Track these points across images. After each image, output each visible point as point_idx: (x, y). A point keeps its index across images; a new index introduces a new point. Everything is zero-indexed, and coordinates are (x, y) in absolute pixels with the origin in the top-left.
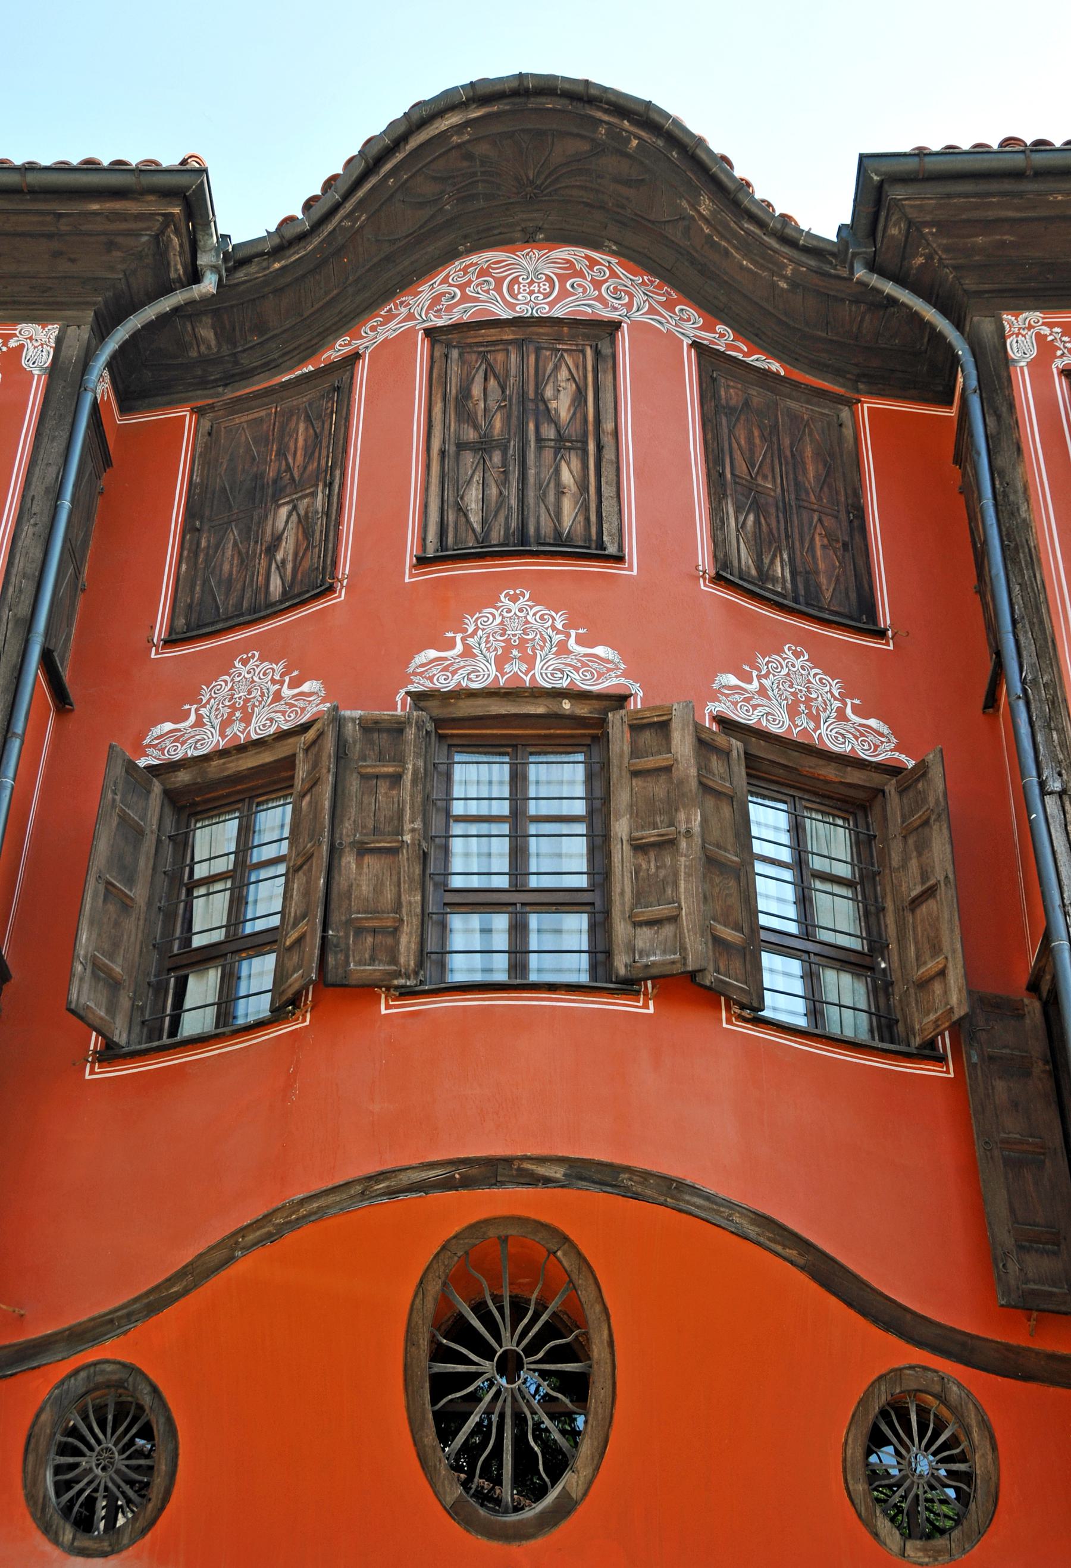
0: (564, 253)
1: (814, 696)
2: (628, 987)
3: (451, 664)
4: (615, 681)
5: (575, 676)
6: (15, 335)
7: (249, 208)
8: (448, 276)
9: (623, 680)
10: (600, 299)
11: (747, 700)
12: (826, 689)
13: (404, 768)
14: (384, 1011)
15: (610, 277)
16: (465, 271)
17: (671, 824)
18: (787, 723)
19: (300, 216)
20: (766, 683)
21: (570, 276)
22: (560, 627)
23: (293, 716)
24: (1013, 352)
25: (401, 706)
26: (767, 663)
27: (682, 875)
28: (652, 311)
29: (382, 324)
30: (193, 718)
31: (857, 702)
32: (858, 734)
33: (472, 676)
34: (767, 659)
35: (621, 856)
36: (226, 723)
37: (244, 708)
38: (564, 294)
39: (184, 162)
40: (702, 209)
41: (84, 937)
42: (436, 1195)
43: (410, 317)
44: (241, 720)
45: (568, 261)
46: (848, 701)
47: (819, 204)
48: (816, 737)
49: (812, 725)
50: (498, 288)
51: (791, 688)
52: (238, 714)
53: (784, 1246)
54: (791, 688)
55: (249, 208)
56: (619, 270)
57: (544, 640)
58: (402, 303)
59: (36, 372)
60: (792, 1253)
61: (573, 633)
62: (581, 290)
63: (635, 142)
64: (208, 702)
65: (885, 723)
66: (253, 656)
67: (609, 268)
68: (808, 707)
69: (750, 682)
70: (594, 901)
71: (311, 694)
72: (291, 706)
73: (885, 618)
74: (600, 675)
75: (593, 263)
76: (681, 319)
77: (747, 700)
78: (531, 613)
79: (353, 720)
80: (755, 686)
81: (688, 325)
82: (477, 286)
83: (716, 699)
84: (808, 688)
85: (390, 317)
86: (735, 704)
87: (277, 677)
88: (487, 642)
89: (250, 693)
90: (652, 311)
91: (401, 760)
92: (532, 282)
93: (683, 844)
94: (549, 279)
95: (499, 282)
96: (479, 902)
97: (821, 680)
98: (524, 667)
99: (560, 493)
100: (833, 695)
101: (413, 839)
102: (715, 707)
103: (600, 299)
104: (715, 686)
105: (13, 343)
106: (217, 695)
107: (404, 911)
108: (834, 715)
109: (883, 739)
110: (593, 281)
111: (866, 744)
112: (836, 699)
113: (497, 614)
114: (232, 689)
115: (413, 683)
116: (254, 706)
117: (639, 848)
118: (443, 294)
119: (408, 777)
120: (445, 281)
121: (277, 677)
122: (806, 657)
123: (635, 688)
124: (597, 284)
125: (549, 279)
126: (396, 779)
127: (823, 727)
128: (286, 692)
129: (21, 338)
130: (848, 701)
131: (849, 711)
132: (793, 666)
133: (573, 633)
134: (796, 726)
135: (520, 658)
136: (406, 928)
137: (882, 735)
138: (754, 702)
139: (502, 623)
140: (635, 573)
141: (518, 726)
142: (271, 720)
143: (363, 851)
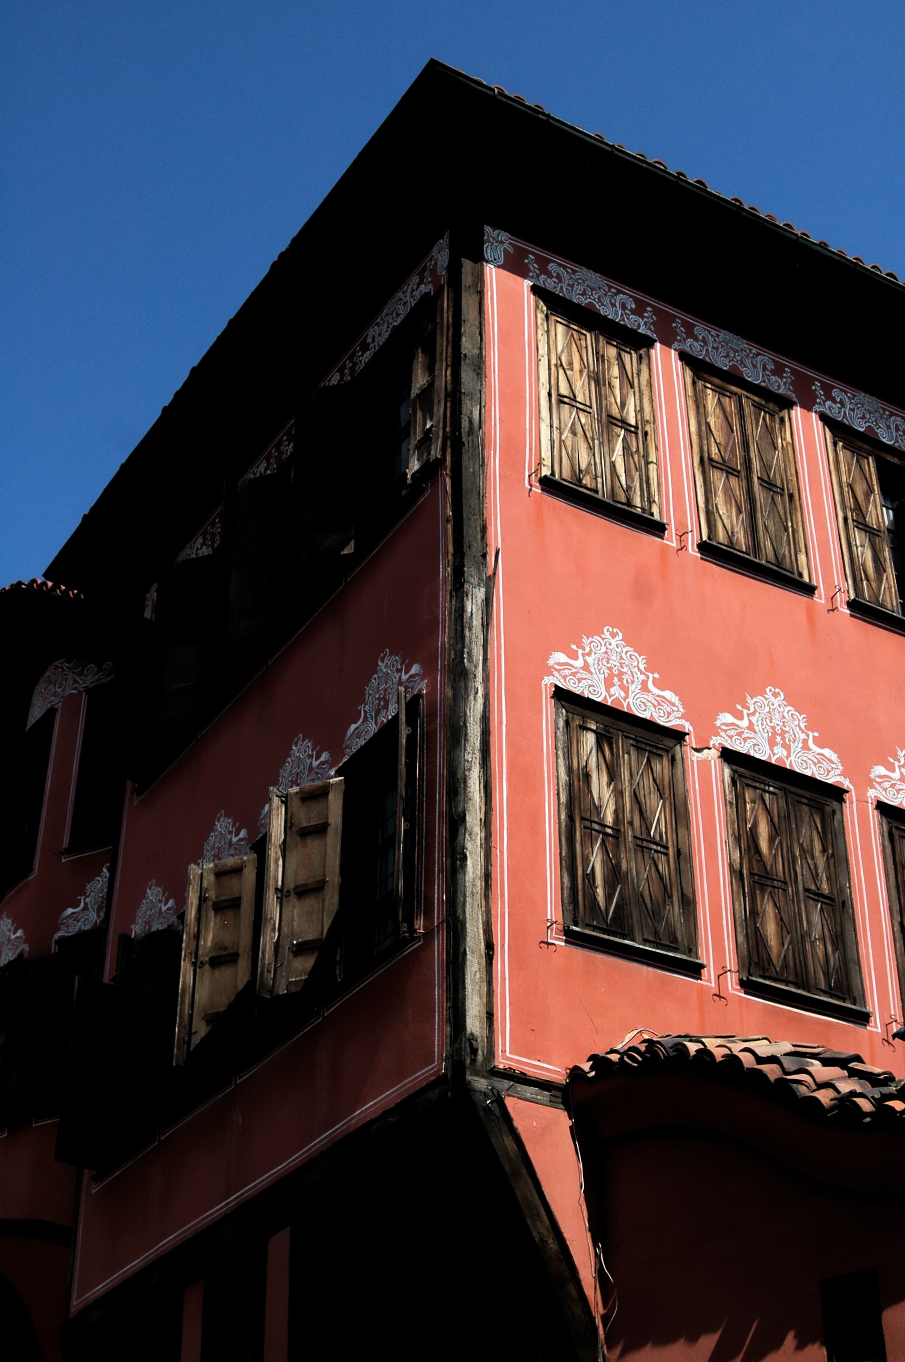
1: (787, 729)
11: (739, 734)
12: (635, 664)
20: (753, 719)
26: (590, 643)
31: (816, 734)
32: (656, 703)
34: (590, 639)
48: (625, 705)
49: (623, 694)
65: (835, 752)
68: (621, 680)
69: (742, 719)
77: (574, 674)
80: (579, 663)
83: (717, 734)
84: (621, 663)
97: (792, 715)
100: (639, 670)
108: (801, 745)
109: (834, 766)
111: (822, 769)
122: (621, 637)
127: (631, 696)
131: (650, 685)
132: (610, 644)
134: (611, 696)
137: (674, 705)
138: (897, 787)
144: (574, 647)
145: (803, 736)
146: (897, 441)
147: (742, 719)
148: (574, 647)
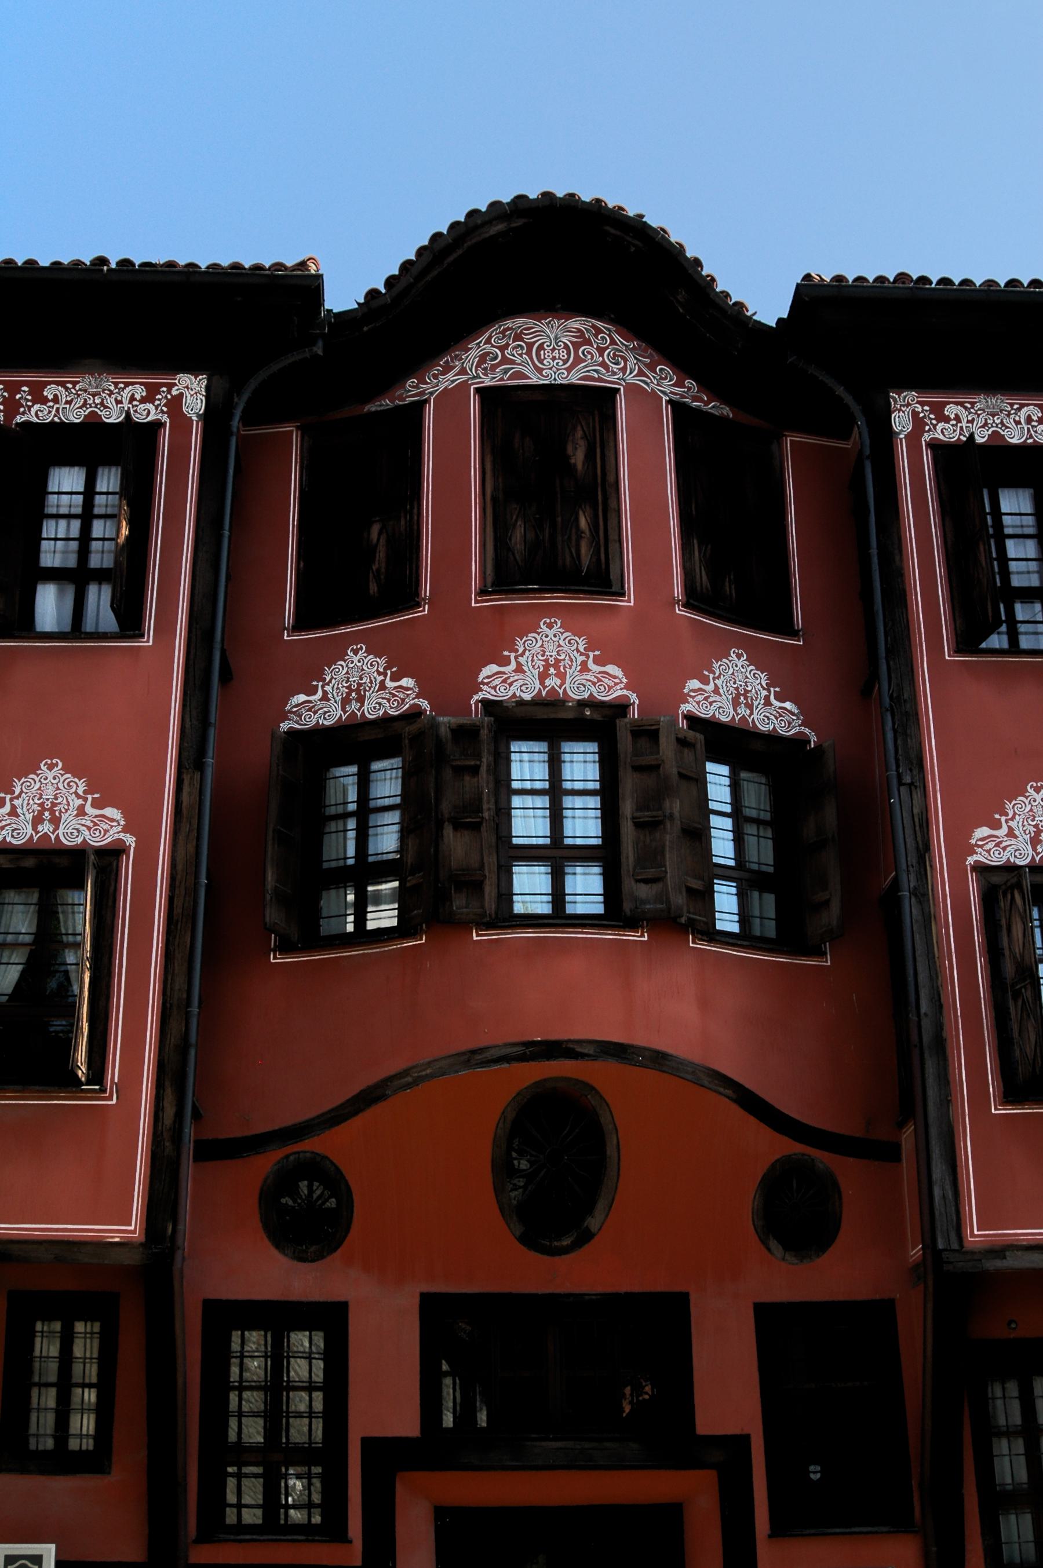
0: (576, 323)
1: (749, 688)
2: (631, 924)
3: (508, 678)
4: (619, 693)
5: (593, 689)
6: (175, 385)
7: (341, 296)
8: (490, 337)
9: (625, 692)
10: (603, 364)
12: (757, 682)
13: (481, 762)
14: (475, 938)
15: (611, 344)
16: (503, 332)
17: (660, 808)
18: (732, 712)
19: (383, 291)
20: (719, 682)
21: (581, 344)
22: (582, 650)
23: (396, 704)
24: (896, 428)
25: (475, 713)
27: (667, 849)
28: (641, 373)
29: (444, 373)
30: (320, 693)
31: (778, 689)
32: (596, 680)
33: (523, 688)
35: (628, 831)
36: (346, 701)
37: (358, 691)
38: (578, 360)
39: (303, 265)
40: (679, 297)
41: (270, 876)
42: (516, 1065)
43: (463, 371)
44: (357, 700)
45: (579, 330)
46: (772, 689)
47: (769, 305)
50: (529, 353)
51: (735, 687)
52: (354, 694)
53: (725, 1088)
54: (735, 687)
55: (341, 296)
56: (617, 338)
57: (571, 660)
58: (457, 356)
59: (195, 418)
60: (728, 1092)
61: (591, 654)
62: (589, 357)
63: (633, 249)
64: (19, 795)
66: (361, 648)
67: (610, 336)
68: (746, 698)
69: (708, 684)
70: (606, 855)
71: (408, 689)
72: (394, 696)
73: (799, 621)
74: (610, 688)
75: (599, 331)
76: (661, 378)
78: (562, 638)
79: (444, 723)
81: (666, 382)
82: (514, 348)
85: (447, 369)
86: (698, 703)
87: (381, 670)
88: (533, 661)
89: (361, 679)
90: (641, 373)
91: (479, 757)
92: (553, 350)
93: (668, 825)
94: (566, 347)
95: (530, 346)
96: (531, 854)
98: (558, 682)
99: (579, 538)
101: (489, 815)
102: (685, 708)
103: (603, 364)
104: (686, 691)
105: (174, 392)
106: (338, 677)
107: (486, 868)
108: (762, 702)
109: (617, 681)
110: (599, 349)
112: (764, 689)
113: (539, 638)
114: (347, 673)
115: (482, 690)
116: (365, 690)
117: (639, 825)
118: (488, 353)
119: (484, 769)
120: (488, 341)
121: (381, 670)
123: (634, 698)
124: (601, 351)
125: (566, 347)
126: (475, 771)
127: (755, 712)
128: (389, 684)
129: (180, 387)
130: (772, 689)
131: (590, 664)
133: (591, 654)
134: (738, 714)
135: (555, 675)
136: (487, 882)
138: (711, 699)
139: (542, 646)
140: (632, 604)
141: (550, 722)
142: (380, 704)
143: (458, 826)
144: (706, 673)
145: (764, 693)
146: (1031, 437)
147: (708, 684)
148: (706, 673)
